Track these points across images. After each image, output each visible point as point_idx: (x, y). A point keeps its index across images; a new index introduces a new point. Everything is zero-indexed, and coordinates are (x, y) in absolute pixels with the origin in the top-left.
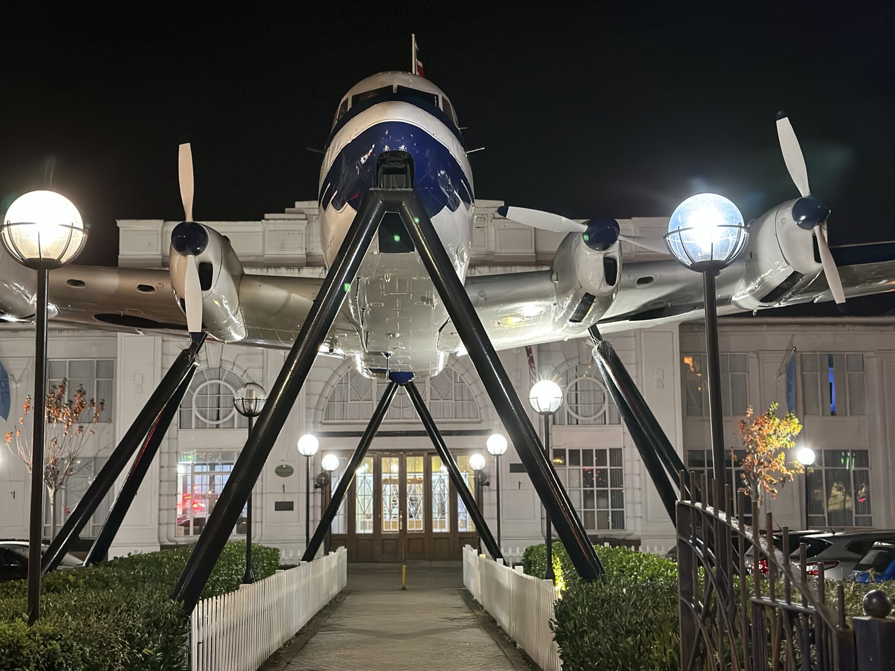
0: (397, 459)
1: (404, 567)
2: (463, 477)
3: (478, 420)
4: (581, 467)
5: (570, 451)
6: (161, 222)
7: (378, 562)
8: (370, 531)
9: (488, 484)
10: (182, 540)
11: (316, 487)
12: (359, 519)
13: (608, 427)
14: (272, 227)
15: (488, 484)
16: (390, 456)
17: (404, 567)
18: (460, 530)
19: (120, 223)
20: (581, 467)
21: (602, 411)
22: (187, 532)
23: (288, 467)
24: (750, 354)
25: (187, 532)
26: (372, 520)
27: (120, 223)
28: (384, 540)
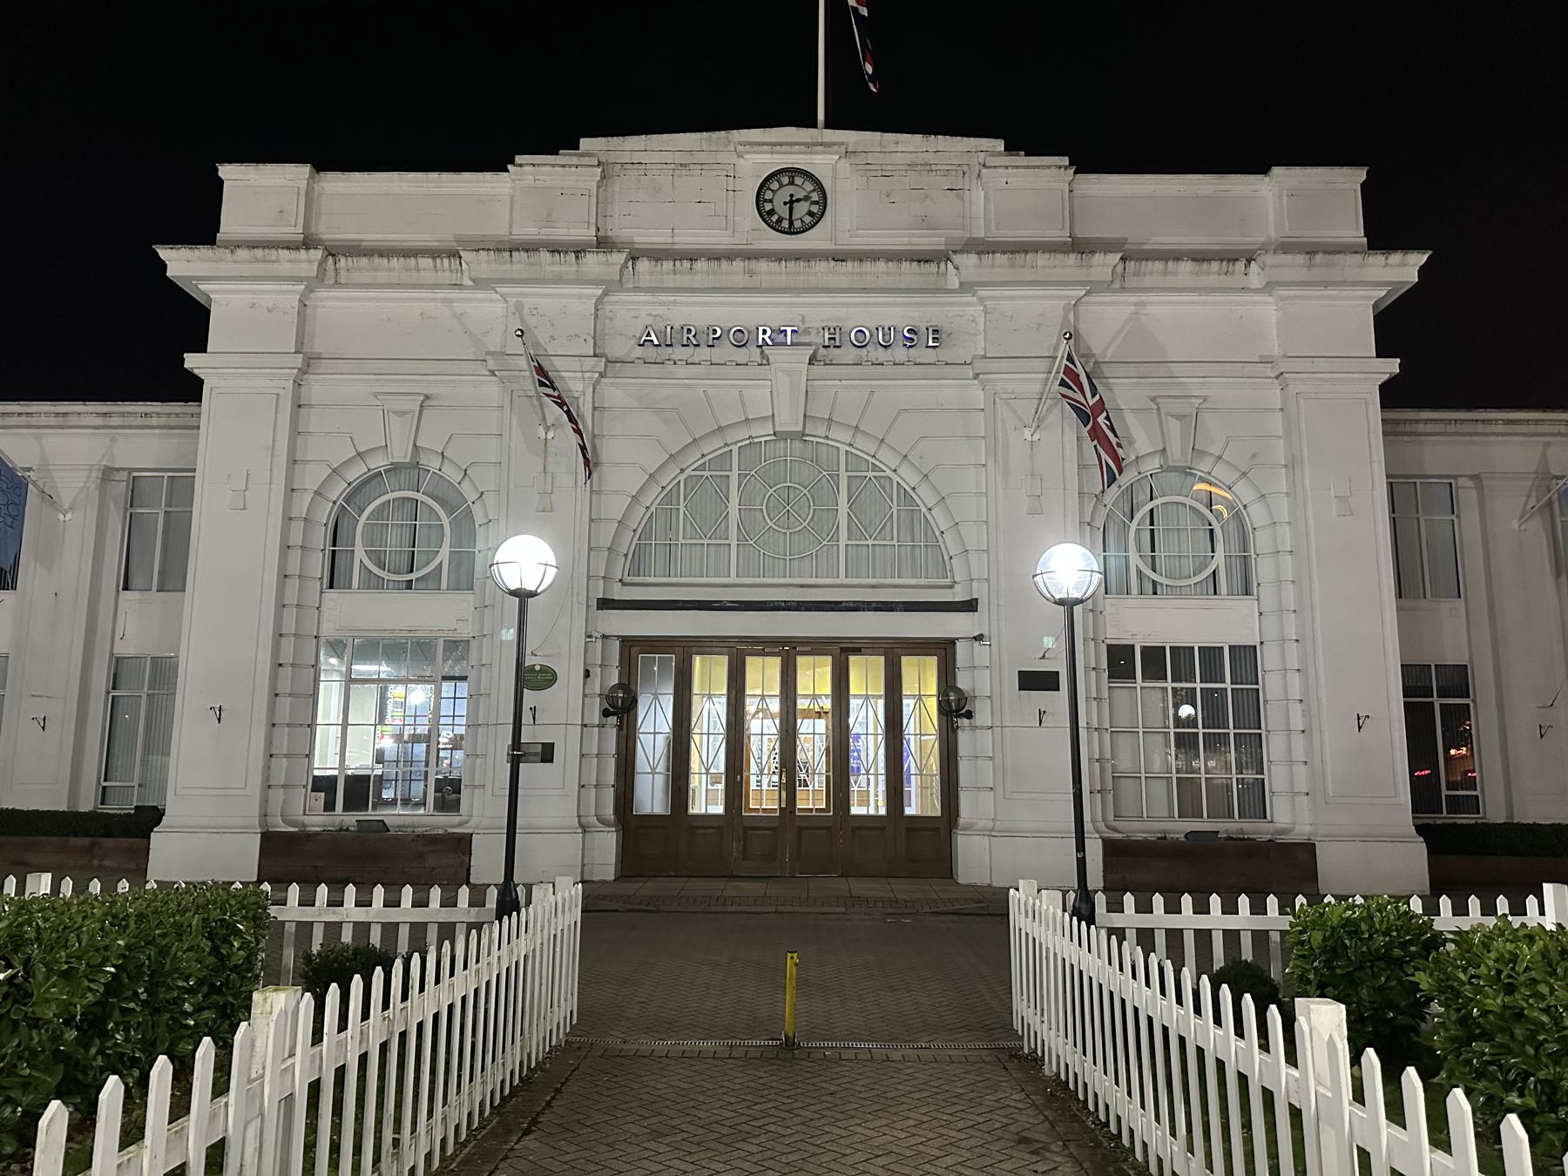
0: (778, 660)
1: (792, 960)
2: (906, 711)
3: (947, 581)
4: (1169, 685)
5: (1145, 650)
6: (305, 170)
7: (731, 877)
8: (718, 809)
9: (969, 715)
10: (318, 821)
11: (606, 713)
12: (697, 782)
13: (1213, 602)
14: (529, 180)
15: (969, 715)
16: (763, 654)
17: (792, 960)
18: (856, 810)
19: (226, 171)
20: (1169, 685)
21: (1209, 571)
22: (330, 806)
23: (545, 670)
24: (1461, 482)
25: (330, 806)
26: (721, 787)
27: (226, 171)
28: (746, 829)
